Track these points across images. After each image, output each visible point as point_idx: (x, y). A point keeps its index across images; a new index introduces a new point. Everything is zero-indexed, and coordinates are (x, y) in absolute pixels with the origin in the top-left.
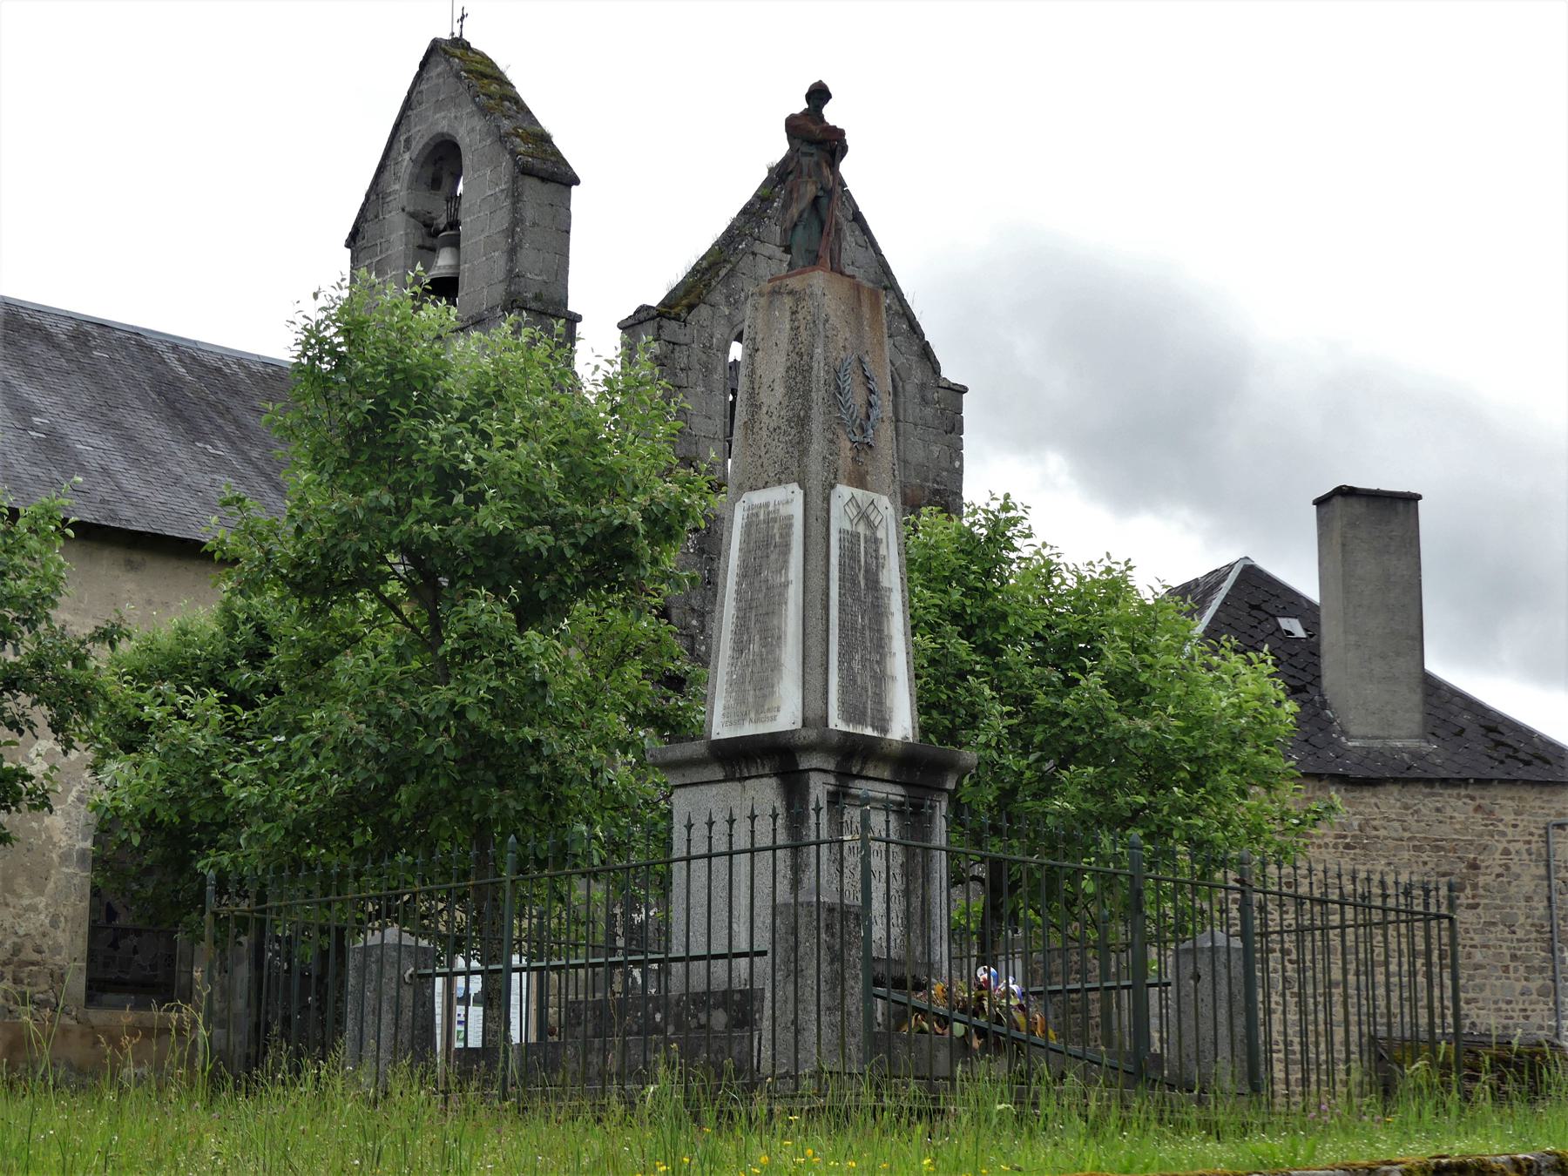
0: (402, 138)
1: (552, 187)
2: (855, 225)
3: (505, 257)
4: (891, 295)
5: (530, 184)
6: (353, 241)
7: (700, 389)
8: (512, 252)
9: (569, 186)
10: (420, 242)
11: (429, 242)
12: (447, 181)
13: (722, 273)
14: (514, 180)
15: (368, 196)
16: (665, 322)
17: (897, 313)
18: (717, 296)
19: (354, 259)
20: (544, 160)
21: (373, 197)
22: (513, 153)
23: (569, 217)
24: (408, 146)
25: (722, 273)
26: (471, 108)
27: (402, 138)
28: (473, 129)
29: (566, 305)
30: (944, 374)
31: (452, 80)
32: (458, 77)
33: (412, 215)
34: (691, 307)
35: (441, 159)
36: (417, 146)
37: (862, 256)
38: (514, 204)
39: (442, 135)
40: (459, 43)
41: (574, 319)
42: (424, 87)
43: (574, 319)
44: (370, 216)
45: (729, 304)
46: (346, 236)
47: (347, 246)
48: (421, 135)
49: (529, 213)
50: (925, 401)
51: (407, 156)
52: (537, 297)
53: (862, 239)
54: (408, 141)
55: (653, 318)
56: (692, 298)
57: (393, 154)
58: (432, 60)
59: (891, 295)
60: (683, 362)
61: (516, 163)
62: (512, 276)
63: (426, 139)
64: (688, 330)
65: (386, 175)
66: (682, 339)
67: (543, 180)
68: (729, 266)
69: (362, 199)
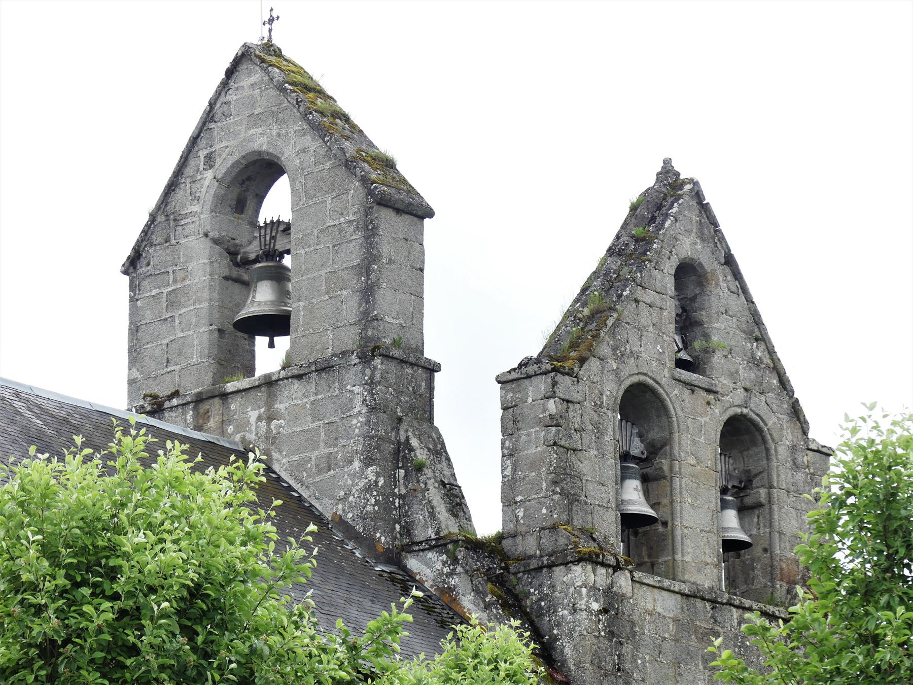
0: (202, 154)
1: (407, 219)
2: (727, 269)
3: (356, 297)
4: (762, 347)
5: (386, 217)
6: (133, 263)
7: (593, 452)
8: (368, 292)
9: (422, 218)
10: (227, 273)
11: (235, 272)
12: (250, 204)
13: (610, 322)
14: (368, 211)
15: (153, 217)
16: (559, 378)
17: (768, 367)
18: (605, 349)
19: (132, 287)
20: (399, 190)
21: (160, 218)
22: (364, 180)
23: (423, 253)
24: (210, 160)
25: (610, 322)
26: (300, 125)
27: (202, 154)
28: (304, 150)
29: (422, 353)
30: (811, 435)
31: (273, 92)
32: (282, 90)
33: (216, 241)
34: (582, 361)
35: (249, 178)
36: (223, 165)
37: (736, 303)
38: (367, 238)
39: (260, 153)
40: (269, 47)
41: (432, 368)
42: (231, 97)
43: (432, 368)
44: (157, 238)
45: (616, 357)
46: (124, 259)
47: (125, 272)
48: (229, 150)
49: (386, 249)
50: (796, 466)
51: (209, 174)
52: (396, 344)
53: (734, 285)
54: (210, 158)
55: (546, 373)
56: (582, 351)
57: (189, 171)
58: (243, 67)
59: (762, 347)
60: (577, 422)
61: (370, 193)
62: (368, 319)
63: (236, 157)
64: (580, 387)
65: (180, 195)
66: (576, 397)
67: (398, 211)
68: (615, 315)
69: (145, 219)
